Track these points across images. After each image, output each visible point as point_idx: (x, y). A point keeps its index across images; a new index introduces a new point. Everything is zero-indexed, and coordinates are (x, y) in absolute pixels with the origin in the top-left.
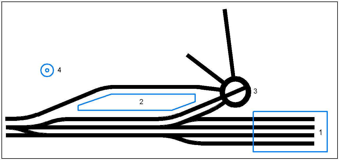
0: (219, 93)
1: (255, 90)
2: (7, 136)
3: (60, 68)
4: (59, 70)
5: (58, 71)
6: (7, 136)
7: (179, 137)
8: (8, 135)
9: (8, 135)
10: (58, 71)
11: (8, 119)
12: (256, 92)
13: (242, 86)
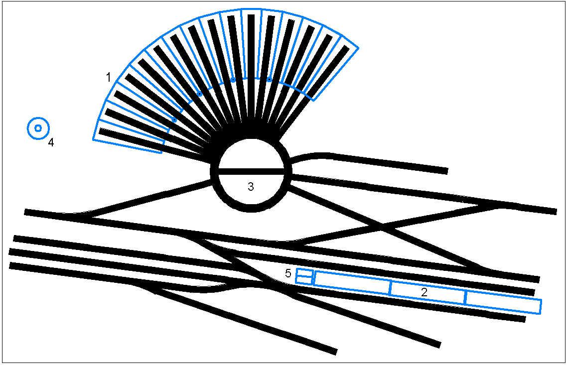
0: (294, 172)
1: (251, 184)
2: (10, 268)
3: (52, 139)
4: (51, 143)
5: (49, 144)
6: (10, 268)
7: (156, 288)
8: (14, 266)
9: (14, 266)
10: (49, 144)
11: (17, 239)
12: (251, 188)
13: (220, 176)
